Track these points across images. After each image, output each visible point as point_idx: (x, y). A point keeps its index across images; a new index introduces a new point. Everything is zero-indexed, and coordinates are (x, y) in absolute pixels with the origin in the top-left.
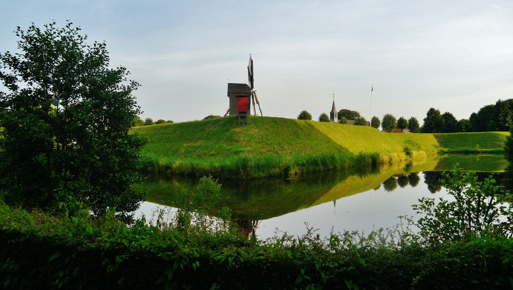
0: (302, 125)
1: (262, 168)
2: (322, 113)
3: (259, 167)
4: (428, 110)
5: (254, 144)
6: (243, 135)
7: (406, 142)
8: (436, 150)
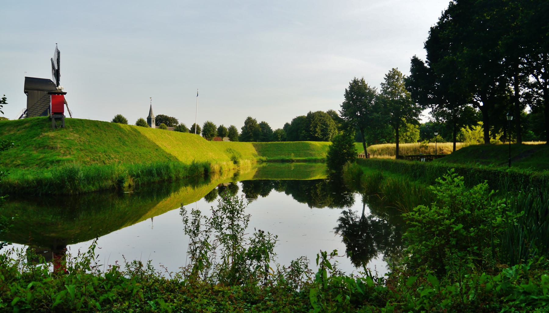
0: (127, 131)
1: (92, 180)
2: (139, 118)
3: (89, 179)
4: (245, 119)
5: (75, 152)
6: (60, 141)
7: (227, 151)
8: (255, 159)
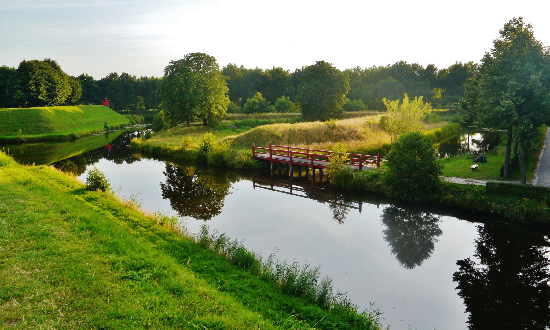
6: (170, 300)
